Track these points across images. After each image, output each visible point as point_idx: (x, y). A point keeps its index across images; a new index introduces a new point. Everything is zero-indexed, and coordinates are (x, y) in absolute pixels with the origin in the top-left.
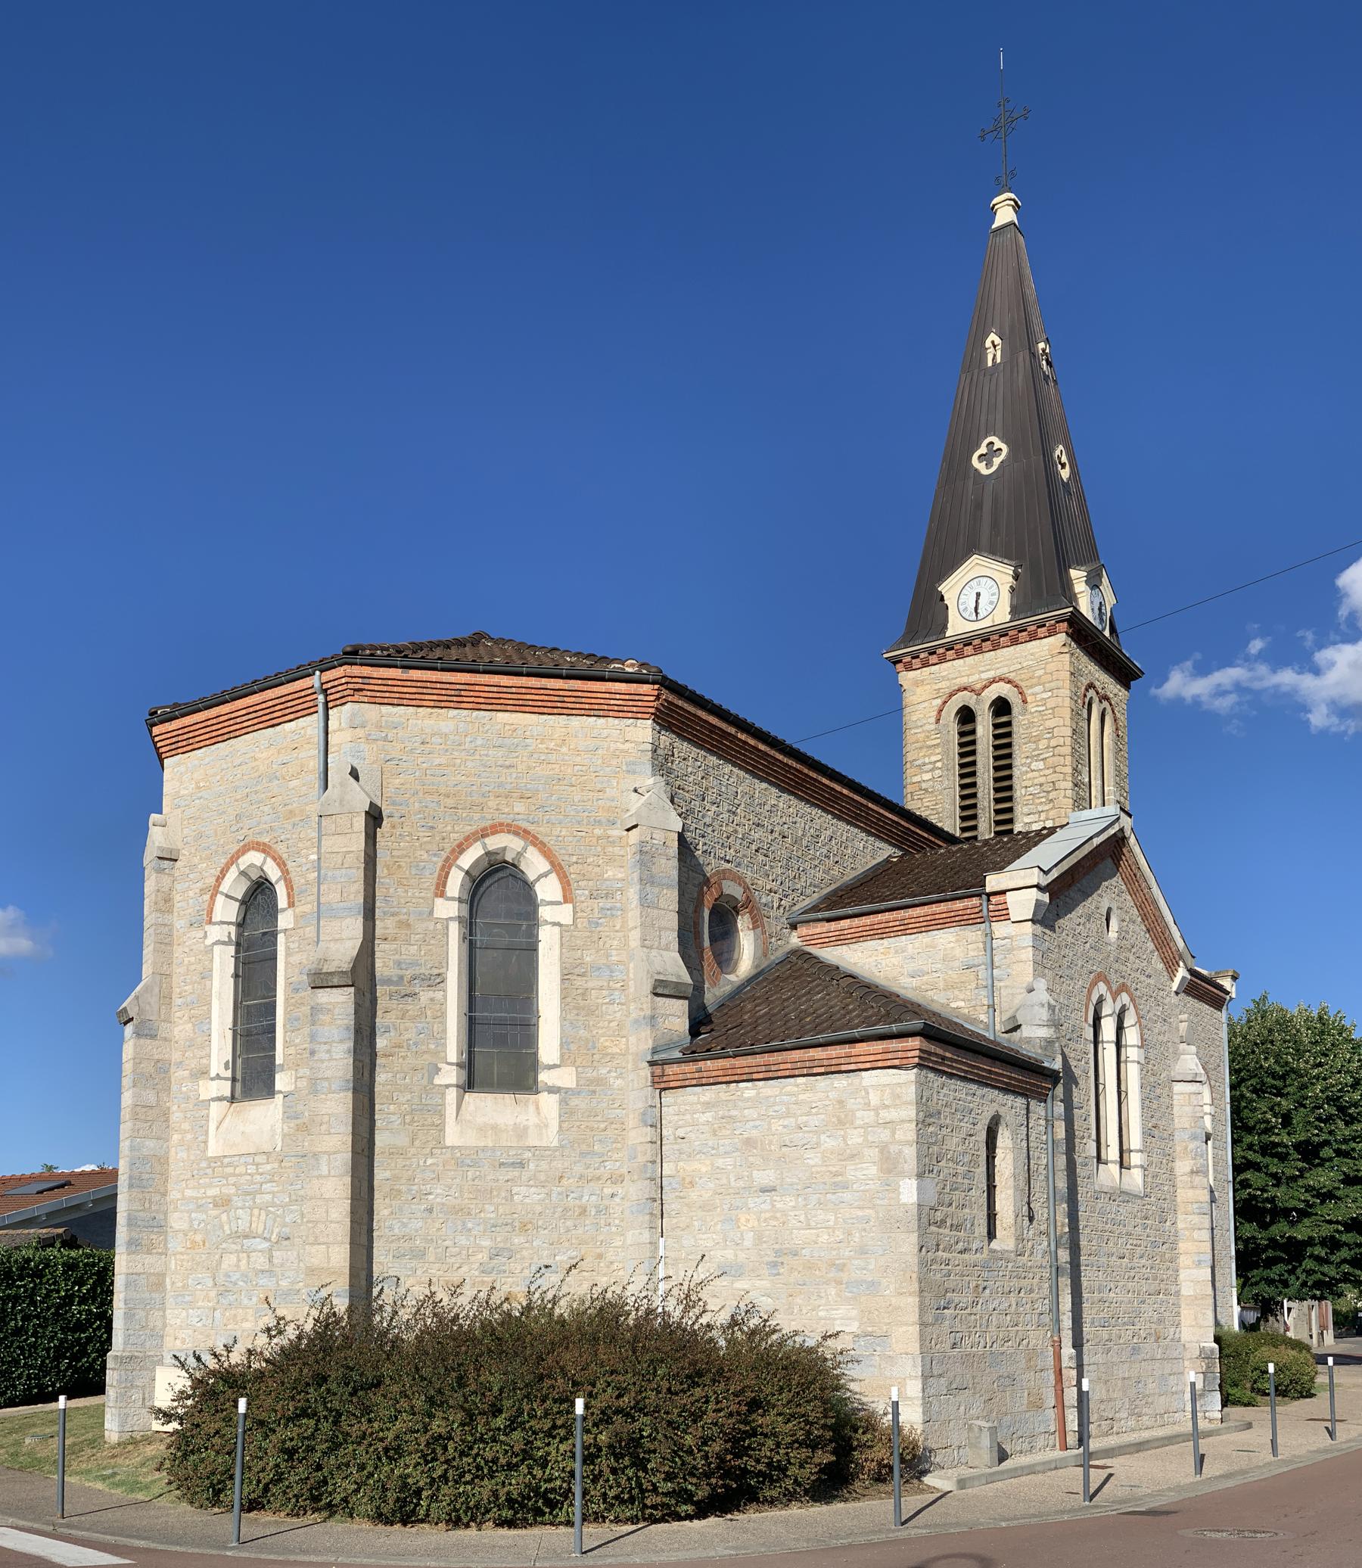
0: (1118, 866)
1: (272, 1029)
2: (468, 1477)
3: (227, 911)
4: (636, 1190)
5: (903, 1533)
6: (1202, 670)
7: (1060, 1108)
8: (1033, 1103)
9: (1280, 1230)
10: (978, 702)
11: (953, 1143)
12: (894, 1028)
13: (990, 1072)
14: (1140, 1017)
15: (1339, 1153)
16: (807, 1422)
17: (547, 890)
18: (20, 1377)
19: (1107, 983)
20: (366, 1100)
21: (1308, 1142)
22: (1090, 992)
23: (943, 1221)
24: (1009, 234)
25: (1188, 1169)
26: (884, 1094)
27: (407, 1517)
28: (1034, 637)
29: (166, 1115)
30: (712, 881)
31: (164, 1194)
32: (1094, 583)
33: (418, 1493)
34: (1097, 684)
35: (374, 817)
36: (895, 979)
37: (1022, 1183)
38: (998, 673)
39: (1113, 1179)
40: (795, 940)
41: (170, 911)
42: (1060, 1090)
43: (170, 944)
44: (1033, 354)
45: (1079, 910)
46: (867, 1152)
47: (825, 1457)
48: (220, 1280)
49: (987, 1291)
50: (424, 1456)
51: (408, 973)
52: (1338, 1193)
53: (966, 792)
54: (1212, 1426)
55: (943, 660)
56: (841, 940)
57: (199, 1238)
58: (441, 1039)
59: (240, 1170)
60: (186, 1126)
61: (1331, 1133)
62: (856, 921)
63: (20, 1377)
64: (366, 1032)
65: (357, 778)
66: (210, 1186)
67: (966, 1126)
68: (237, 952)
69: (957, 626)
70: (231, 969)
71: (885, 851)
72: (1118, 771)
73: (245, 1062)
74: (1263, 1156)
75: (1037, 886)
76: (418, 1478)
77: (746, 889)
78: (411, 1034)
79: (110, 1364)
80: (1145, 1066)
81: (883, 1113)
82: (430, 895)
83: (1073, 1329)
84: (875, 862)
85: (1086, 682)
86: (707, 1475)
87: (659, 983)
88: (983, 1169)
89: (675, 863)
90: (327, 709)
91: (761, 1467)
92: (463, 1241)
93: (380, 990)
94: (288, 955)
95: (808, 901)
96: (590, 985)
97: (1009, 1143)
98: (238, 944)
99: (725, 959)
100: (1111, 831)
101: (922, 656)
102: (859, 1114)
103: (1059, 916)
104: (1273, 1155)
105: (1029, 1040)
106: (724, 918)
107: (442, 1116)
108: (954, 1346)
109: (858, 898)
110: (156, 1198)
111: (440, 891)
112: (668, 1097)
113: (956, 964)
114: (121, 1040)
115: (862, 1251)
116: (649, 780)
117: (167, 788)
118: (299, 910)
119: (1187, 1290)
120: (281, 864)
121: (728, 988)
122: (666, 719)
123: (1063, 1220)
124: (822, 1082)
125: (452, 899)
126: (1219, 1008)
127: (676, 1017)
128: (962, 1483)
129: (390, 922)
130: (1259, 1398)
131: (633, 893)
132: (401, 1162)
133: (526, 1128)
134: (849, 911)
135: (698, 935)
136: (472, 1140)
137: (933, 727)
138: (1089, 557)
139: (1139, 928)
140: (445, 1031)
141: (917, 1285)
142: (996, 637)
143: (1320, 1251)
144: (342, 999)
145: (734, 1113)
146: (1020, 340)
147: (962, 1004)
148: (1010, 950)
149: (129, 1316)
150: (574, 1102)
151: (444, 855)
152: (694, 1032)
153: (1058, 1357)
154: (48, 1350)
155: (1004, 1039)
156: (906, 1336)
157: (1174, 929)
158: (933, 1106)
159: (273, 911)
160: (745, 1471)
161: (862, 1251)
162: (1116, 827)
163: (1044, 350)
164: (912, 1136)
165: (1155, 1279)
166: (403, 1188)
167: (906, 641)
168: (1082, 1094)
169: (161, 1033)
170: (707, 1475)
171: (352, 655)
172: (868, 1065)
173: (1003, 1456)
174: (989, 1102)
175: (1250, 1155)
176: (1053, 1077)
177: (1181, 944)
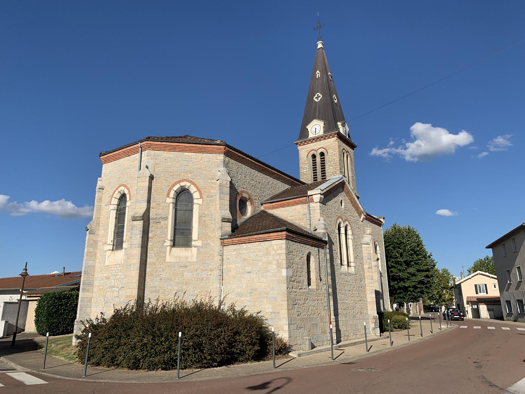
0: (343, 189)
1: (123, 232)
2: (153, 355)
3: (115, 202)
4: (217, 273)
5: (180, 381)
6: (380, 148)
7: (328, 251)
8: (320, 249)
9: (402, 284)
11: (297, 259)
12: (279, 229)
14: (351, 228)
15: (415, 263)
16: (251, 338)
17: (196, 195)
18: (61, 327)
19: (342, 218)
20: (145, 250)
21: (407, 260)
22: (337, 221)
23: (294, 281)
26: (277, 246)
28: (329, 138)
29: (95, 255)
32: (343, 125)
33: (139, 360)
35: (152, 178)
37: (318, 271)
38: (321, 146)
40: (262, 208)
41: (101, 202)
42: (328, 246)
44: (327, 75)
45: (333, 200)
46: (273, 262)
47: (257, 348)
48: (106, 299)
50: (141, 350)
51: (159, 217)
54: (377, 338)
55: (308, 143)
56: (273, 208)
57: (101, 287)
58: (166, 234)
59: (113, 269)
60: (100, 257)
61: (413, 258)
63: (61, 327)
64: (146, 232)
65: (148, 168)
66: (105, 273)
67: (301, 255)
69: (311, 135)
71: (287, 187)
72: (352, 169)
73: (117, 240)
74: (396, 264)
76: (139, 356)
77: (249, 195)
79: (75, 323)
80: (354, 240)
81: (277, 251)
83: (334, 311)
86: (221, 354)
87: (223, 218)
89: (229, 189)
90: (142, 152)
91: (238, 351)
92: (169, 287)
94: (128, 212)
96: (206, 219)
98: (117, 210)
99: (243, 213)
100: (341, 181)
103: (327, 202)
104: (399, 264)
105: (319, 233)
106: (243, 203)
107: (165, 254)
109: (279, 198)
110: (91, 277)
111: (168, 196)
112: (225, 248)
114: (86, 235)
115: (273, 289)
116: (222, 169)
117: (103, 172)
118: (132, 201)
119: (369, 300)
120: (128, 189)
121: (244, 220)
122: (227, 154)
123: (330, 280)
124: (262, 243)
127: (228, 227)
128: (299, 355)
130: (394, 329)
131: (218, 196)
132: (154, 266)
133: (188, 257)
134: (275, 200)
135: (236, 207)
136: (173, 260)
139: (350, 206)
141: (286, 298)
143: (411, 289)
146: (324, 72)
147: (303, 224)
148: (314, 210)
149: (81, 310)
150: (201, 250)
152: (233, 231)
153: (330, 319)
154: (70, 319)
155: (313, 233)
156: (284, 313)
157: (360, 205)
159: (126, 201)
160: (233, 353)
161: (273, 289)
162: (342, 180)
164: (285, 258)
167: (299, 139)
168: (336, 247)
170: (221, 354)
171: (148, 139)
173: (313, 347)
174: (308, 249)
175: (393, 264)
176: (326, 242)
177: (362, 209)
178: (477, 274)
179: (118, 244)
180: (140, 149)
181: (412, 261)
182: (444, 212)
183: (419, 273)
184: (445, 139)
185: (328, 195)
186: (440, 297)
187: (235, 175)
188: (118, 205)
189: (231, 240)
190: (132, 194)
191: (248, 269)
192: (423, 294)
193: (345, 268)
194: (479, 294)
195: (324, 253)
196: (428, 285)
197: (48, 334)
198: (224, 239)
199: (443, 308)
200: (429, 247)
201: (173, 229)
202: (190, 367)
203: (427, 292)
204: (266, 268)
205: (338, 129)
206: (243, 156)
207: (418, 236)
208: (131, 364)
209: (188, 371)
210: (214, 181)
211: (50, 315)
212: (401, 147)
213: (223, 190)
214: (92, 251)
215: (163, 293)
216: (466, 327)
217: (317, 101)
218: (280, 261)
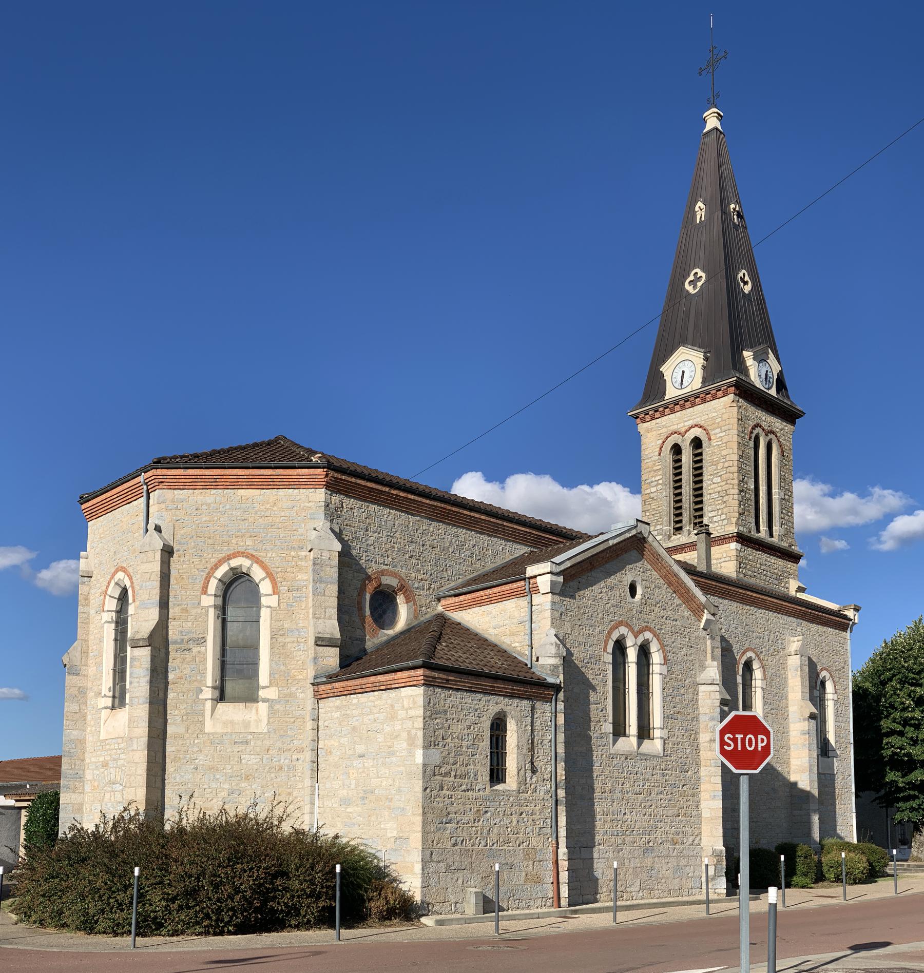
3: (112, 605)
4: (308, 756)
8: (538, 704)
10: (683, 441)
11: (457, 728)
12: (410, 663)
13: (493, 687)
14: (663, 647)
17: (265, 587)
19: (627, 625)
20: (161, 708)
22: (610, 633)
25: (708, 739)
28: (715, 397)
29: (84, 717)
30: (373, 577)
31: (83, 760)
32: (761, 359)
34: (764, 424)
35: (168, 552)
36: (799, 625)
40: (440, 609)
42: (561, 695)
43: (88, 623)
44: (725, 212)
45: (602, 584)
49: (489, 814)
51: (186, 638)
53: (696, 493)
54: (720, 898)
55: (663, 415)
57: (96, 784)
58: (203, 674)
59: (112, 747)
66: (101, 755)
68: (116, 626)
69: (672, 392)
70: (113, 636)
75: (551, 572)
77: (401, 579)
78: (187, 671)
82: (199, 593)
84: (512, 557)
85: (752, 424)
89: (336, 569)
93: (172, 647)
95: (453, 584)
96: (287, 640)
97: (515, 728)
100: (628, 535)
101: (651, 413)
102: (400, 712)
103: (579, 589)
104: (911, 725)
105: (543, 666)
106: (384, 603)
107: (203, 716)
108: (455, 844)
110: (78, 762)
111: (204, 591)
113: (515, 621)
116: (321, 523)
118: (137, 603)
120: (131, 579)
121: (385, 638)
122: (333, 487)
125: (211, 595)
127: (331, 658)
128: (440, 923)
132: (180, 742)
133: (249, 722)
136: (219, 729)
137: (657, 458)
138: (765, 341)
139: (666, 593)
140: (206, 669)
141: (421, 811)
142: (693, 399)
144: (145, 653)
145: (348, 712)
150: (277, 707)
151: (207, 571)
156: (416, 839)
162: (634, 532)
163: (734, 209)
164: (421, 725)
166: (182, 756)
167: (643, 403)
169: (82, 672)
171: (158, 463)
172: (403, 685)
176: (556, 688)
180: (145, 487)
187: (361, 534)
189: (329, 686)
190: (137, 588)
191: (360, 749)
193: (630, 742)
195: (551, 715)
198: (318, 684)
201: (218, 663)
205: (745, 371)
206: (379, 487)
213: (322, 574)
214: (76, 708)
215: (202, 794)
218: (413, 732)
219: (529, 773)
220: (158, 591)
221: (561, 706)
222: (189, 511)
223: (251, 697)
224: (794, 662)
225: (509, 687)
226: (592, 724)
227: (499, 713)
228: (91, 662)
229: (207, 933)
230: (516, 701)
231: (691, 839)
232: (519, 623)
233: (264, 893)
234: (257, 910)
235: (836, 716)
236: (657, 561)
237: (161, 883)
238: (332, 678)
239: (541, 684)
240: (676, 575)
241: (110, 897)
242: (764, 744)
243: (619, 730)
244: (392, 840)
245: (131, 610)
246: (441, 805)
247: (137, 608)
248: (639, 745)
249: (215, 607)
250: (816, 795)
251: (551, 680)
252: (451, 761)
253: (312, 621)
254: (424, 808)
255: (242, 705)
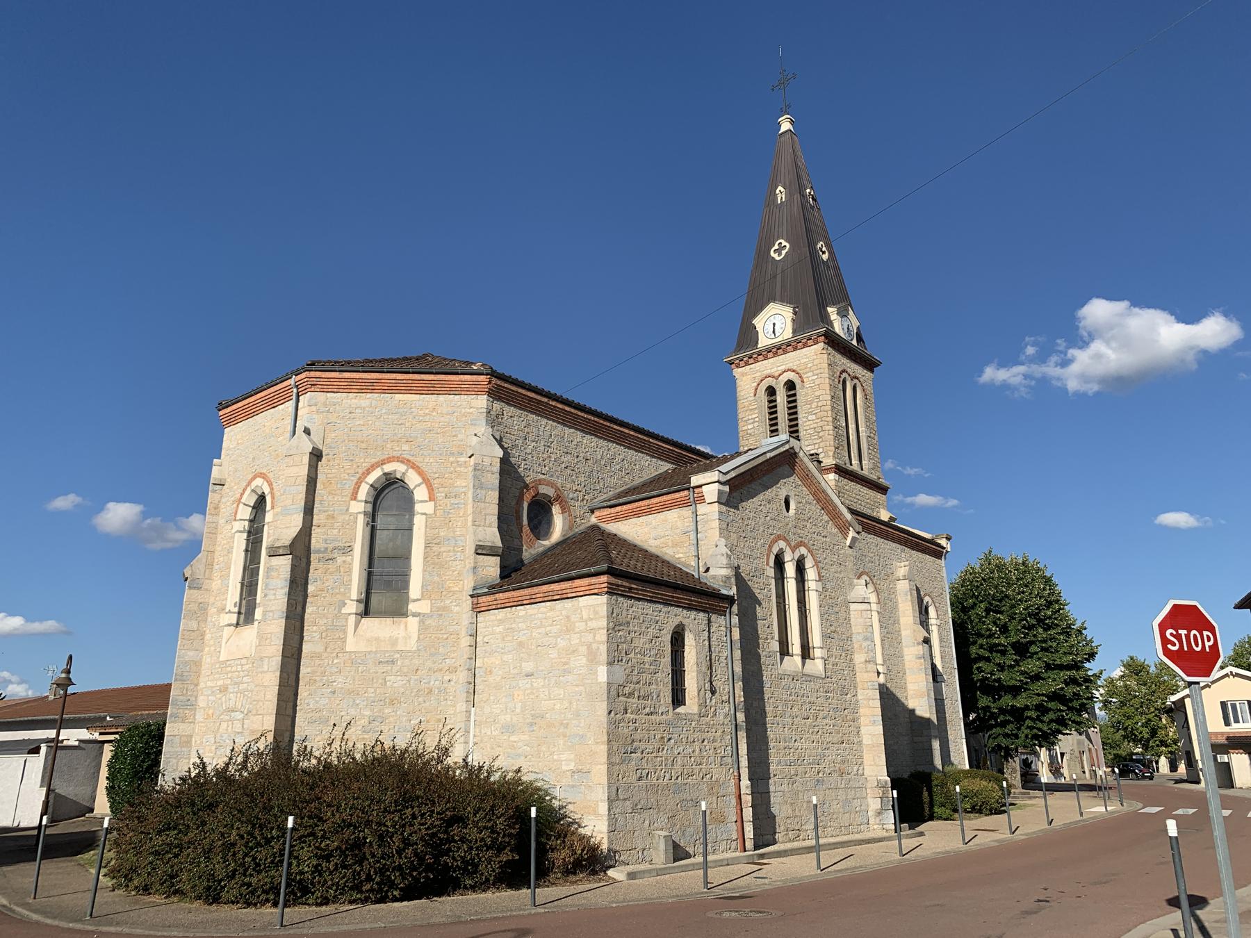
3: (245, 513)
4: (463, 676)
6: (1003, 364)
8: (714, 617)
9: (1007, 701)
11: (640, 642)
12: (592, 569)
14: (817, 563)
15: (1043, 649)
17: (420, 494)
19: (785, 540)
20: (298, 624)
21: (1018, 642)
22: (770, 547)
23: (631, 695)
24: (788, 136)
27: (216, 900)
28: (805, 346)
29: (203, 635)
32: (843, 314)
35: (316, 455)
37: (704, 668)
38: (787, 367)
39: (797, 666)
40: (593, 520)
41: (217, 514)
42: (735, 608)
44: (803, 195)
45: (761, 496)
51: (331, 546)
52: (1045, 675)
54: (885, 834)
56: (617, 518)
62: (625, 507)
65: (309, 434)
66: (219, 679)
67: (653, 631)
69: (764, 342)
71: (665, 467)
72: (867, 419)
76: (220, 872)
77: (557, 489)
80: (822, 594)
81: (590, 624)
88: (667, 660)
90: (298, 396)
98: (249, 532)
100: (782, 449)
103: (742, 501)
104: (997, 651)
105: (714, 577)
106: (540, 511)
107: (345, 632)
108: (640, 779)
112: (481, 617)
116: (483, 429)
118: (277, 510)
119: (866, 740)
120: (270, 485)
121: (541, 549)
122: (495, 394)
126: (940, 558)
127: (491, 567)
128: (632, 876)
129: (323, 516)
132: (317, 662)
136: (362, 647)
138: (845, 303)
139: (814, 509)
141: (605, 738)
143: (1034, 714)
146: (797, 187)
148: (706, 522)
152: (502, 577)
156: (600, 772)
158: (622, 619)
159: (264, 511)
160: (446, 867)
162: (787, 447)
164: (604, 638)
165: (838, 733)
167: (737, 351)
169: (204, 587)
171: (312, 366)
174: (672, 617)
175: (982, 652)
176: (730, 600)
178: (1226, 675)
179: (246, 613)
181: (1032, 643)
182: (1177, 519)
183: (1052, 674)
184: (1166, 336)
185: (741, 488)
186: (1154, 732)
188: (251, 521)
189: (492, 597)
190: (277, 494)
191: (528, 667)
192: (1066, 726)
193: (794, 662)
194: (1234, 726)
195: (726, 627)
196: (1076, 704)
197: (1226, 813)
198: (479, 595)
199: (1164, 763)
200: (1077, 609)
201: (365, 574)
202: (335, 900)
203: (1074, 722)
204: (565, 664)
205: (831, 323)
206: (539, 398)
207: (1048, 581)
208: (200, 889)
209: (330, 908)
210: (463, 459)
211: (404, 776)
212: (1054, 359)
215: (347, 718)
216: (1191, 811)
217: (778, 258)
218: (594, 646)
219: (709, 694)
220: (303, 495)
221: (735, 620)
222: (342, 414)
223: (398, 611)
224: (903, 587)
225: (687, 598)
226: (761, 641)
227: (678, 626)
228: (216, 574)
229: (365, 901)
230: (693, 613)
231: (856, 768)
232: (686, 532)
233: (438, 846)
234: (429, 868)
235: (941, 641)
236: (807, 479)
237: (313, 834)
238: (493, 589)
239: (715, 595)
240: (824, 492)
241: (246, 855)
242: (1211, 643)
243: (784, 651)
244: (569, 773)
245: (269, 517)
246: (626, 731)
247: (274, 515)
248: (803, 664)
249: (365, 513)
250: (935, 721)
251: (724, 592)
252: (635, 680)
253: (471, 529)
254: (609, 735)
255: (389, 620)
